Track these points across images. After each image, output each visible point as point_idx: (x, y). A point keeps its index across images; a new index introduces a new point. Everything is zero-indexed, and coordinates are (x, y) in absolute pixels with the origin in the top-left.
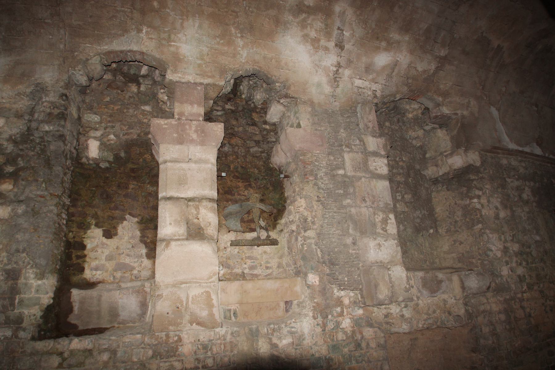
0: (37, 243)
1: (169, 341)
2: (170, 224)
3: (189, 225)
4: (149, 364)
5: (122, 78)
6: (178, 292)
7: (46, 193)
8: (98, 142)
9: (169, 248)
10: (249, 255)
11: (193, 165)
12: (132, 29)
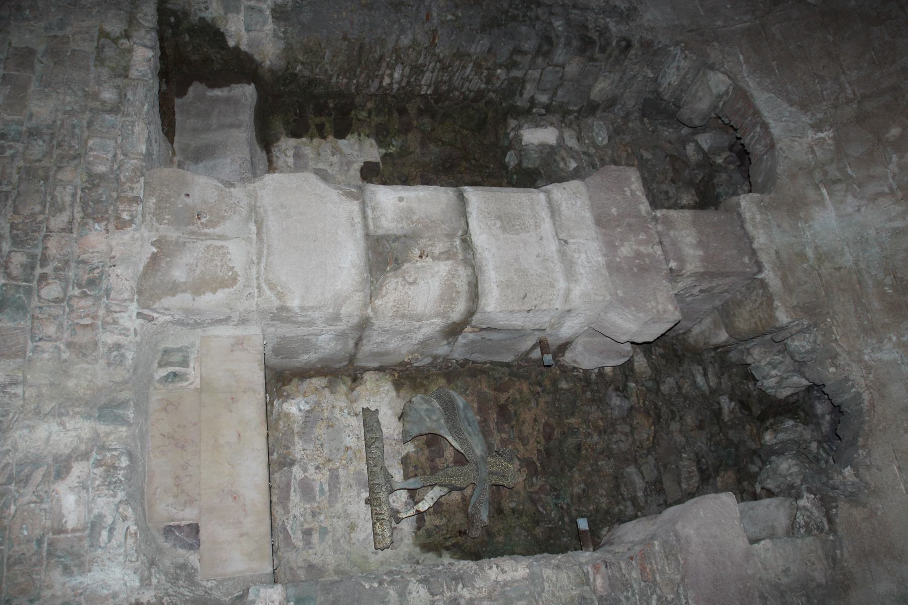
0: (340, 8)
1: (122, 203)
2: (401, 199)
3: (403, 239)
4: (76, 166)
5: (700, 178)
6: (237, 218)
7: (435, 22)
8: (555, 142)
9: (344, 198)
10: (342, 479)
11: (553, 247)
12: (813, 114)
